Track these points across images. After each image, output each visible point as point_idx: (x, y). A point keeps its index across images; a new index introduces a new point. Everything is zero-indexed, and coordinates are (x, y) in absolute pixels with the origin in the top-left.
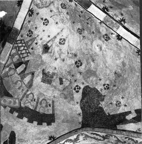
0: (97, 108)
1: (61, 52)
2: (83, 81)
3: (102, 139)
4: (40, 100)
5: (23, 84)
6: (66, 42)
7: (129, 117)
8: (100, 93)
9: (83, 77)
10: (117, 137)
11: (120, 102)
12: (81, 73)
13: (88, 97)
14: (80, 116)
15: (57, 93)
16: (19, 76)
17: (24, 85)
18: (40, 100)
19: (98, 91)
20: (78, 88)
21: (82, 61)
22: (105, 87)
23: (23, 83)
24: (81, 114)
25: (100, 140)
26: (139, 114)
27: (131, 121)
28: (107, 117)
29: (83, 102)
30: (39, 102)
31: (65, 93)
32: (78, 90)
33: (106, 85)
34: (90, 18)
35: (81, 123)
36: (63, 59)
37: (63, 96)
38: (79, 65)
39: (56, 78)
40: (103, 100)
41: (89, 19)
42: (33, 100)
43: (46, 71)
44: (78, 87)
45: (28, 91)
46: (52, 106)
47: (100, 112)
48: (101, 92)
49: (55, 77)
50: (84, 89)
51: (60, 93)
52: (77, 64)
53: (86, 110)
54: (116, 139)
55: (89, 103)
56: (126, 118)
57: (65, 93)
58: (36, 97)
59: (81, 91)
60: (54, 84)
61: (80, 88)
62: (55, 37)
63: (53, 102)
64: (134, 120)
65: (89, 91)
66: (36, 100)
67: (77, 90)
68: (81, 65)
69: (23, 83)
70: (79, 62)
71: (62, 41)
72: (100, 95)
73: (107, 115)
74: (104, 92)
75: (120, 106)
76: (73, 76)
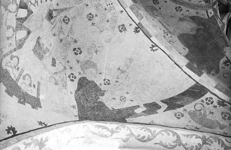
0: (97, 103)
1: (62, 31)
2: (81, 71)
3: (109, 133)
4: (24, 74)
5: (14, 36)
6: (70, 23)
7: (138, 111)
8: (99, 87)
9: (81, 66)
10: (130, 129)
11: (125, 98)
12: (79, 62)
13: (85, 89)
14: (74, 108)
15: (46, 74)
16: (16, 21)
17: (14, 39)
18: (24, 74)
19: (96, 85)
20: (73, 77)
21: (82, 50)
22: (105, 82)
23: (15, 34)
24: (77, 107)
25: (106, 136)
26: (149, 108)
27: (141, 114)
28: (111, 111)
29: (78, 94)
30: (22, 75)
31: (57, 77)
32: (74, 79)
33: (107, 80)
34: (112, 4)
35: (78, 116)
36: (62, 39)
37: (53, 81)
38: (77, 52)
39: (49, 56)
40: (103, 95)
41: (111, 4)
42: (17, 68)
43: (41, 41)
44: (74, 76)
45: (15, 50)
46: (36, 87)
47: (101, 106)
48: (100, 87)
49: (48, 54)
50: (80, 79)
51: (49, 75)
52: (76, 51)
53: (83, 103)
54: (129, 132)
55: (86, 96)
56: (135, 111)
57: (57, 77)
58: (20, 66)
59: (76, 81)
60: (44, 61)
61: (75, 78)
62: (62, 10)
63: (39, 83)
64: (144, 114)
65: (86, 83)
66: (20, 70)
67: (71, 78)
68: (80, 53)
69: (15, 34)
70: (79, 49)
71: (66, 20)
72: (99, 90)
73: (111, 109)
74: (103, 88)
75: (126, 100)
76: (68, 62)
